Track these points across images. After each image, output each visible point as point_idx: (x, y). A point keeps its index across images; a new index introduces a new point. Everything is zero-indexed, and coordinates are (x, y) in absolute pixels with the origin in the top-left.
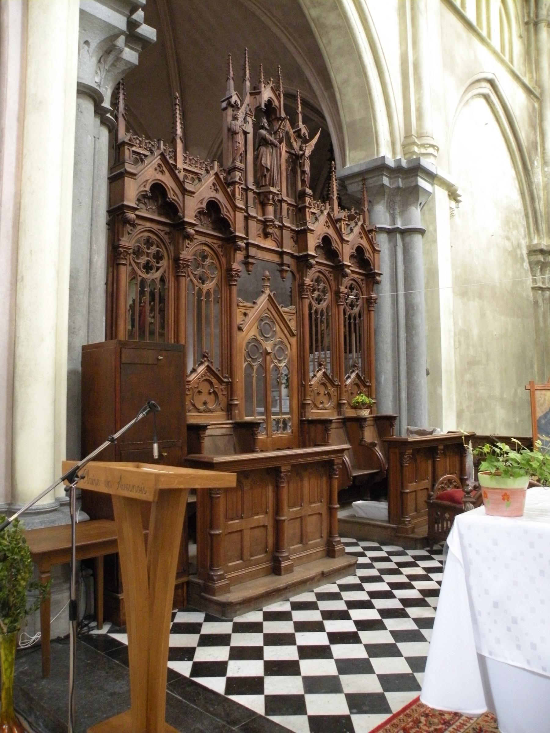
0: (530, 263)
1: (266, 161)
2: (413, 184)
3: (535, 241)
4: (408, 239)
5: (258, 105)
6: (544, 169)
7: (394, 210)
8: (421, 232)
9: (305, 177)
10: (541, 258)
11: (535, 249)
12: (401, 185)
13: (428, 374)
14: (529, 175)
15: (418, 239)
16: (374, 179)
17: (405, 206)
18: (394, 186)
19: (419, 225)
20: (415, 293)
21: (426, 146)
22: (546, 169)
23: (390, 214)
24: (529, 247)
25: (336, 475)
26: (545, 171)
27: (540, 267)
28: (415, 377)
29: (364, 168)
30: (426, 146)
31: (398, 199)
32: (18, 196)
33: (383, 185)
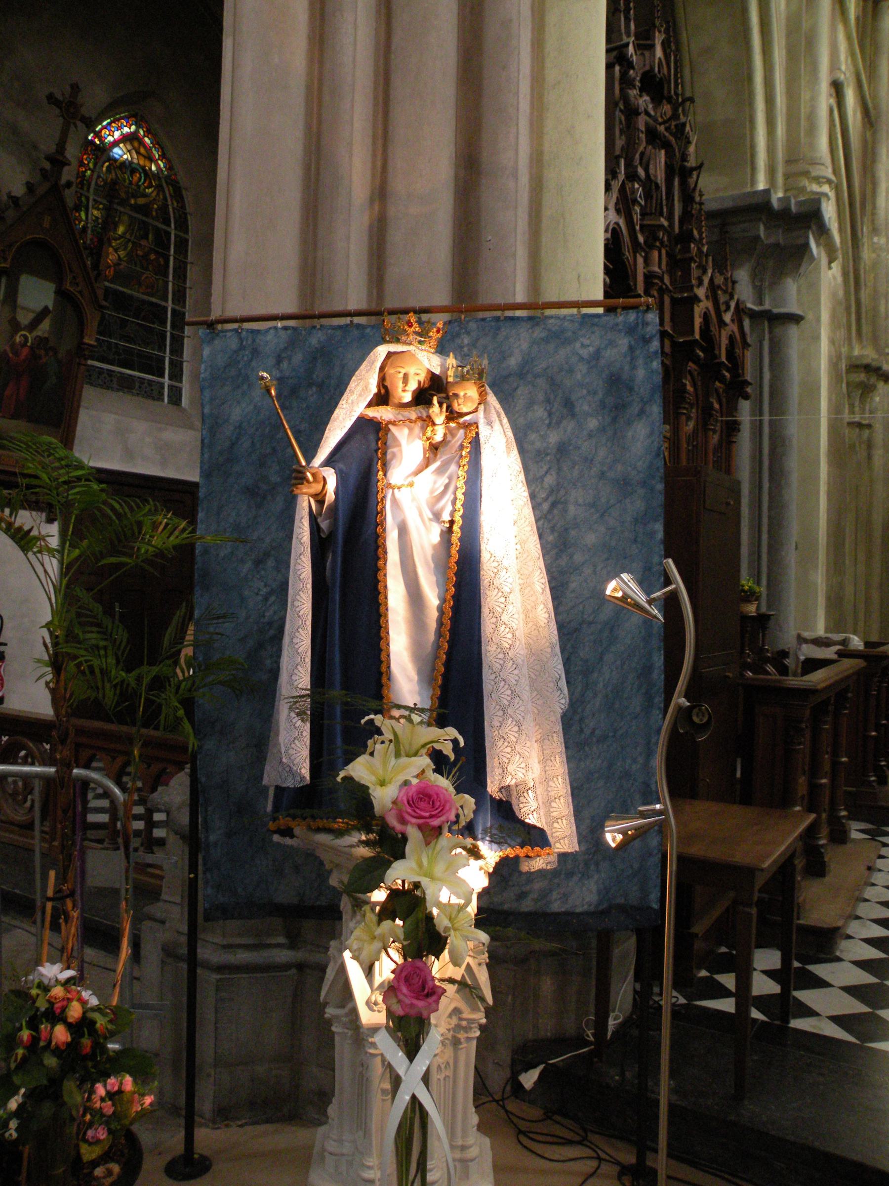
0: (848, 384)
1: (656, 171)
2: (801, 241)
3: (856, 352)
4: (778, 330)
5: (647, 68)
6: (872, 239)
7: (762, 280)
8: (796, 319)
9: (692, 209)
10: (862, 377)
11: (859, 362)
12: (781, 241)
13: (796, 548)
14: (858, 247)
15: (793, 331)
16: (742, 226)
17: (779, 274)
18: (772, 240)
19: (793, 308)
20: (787, 420)
21: (821, 180)
22: (875, 239)
23: (755, 287)
24: (849, 358)
25: (846, 708)
26: (874, 243)
27: (860, 392)
28: (783, 553)
29: (729, 204)
30: (821, 180)
31: (771, 263)
32: (538, 160)
33: (758, 237)
